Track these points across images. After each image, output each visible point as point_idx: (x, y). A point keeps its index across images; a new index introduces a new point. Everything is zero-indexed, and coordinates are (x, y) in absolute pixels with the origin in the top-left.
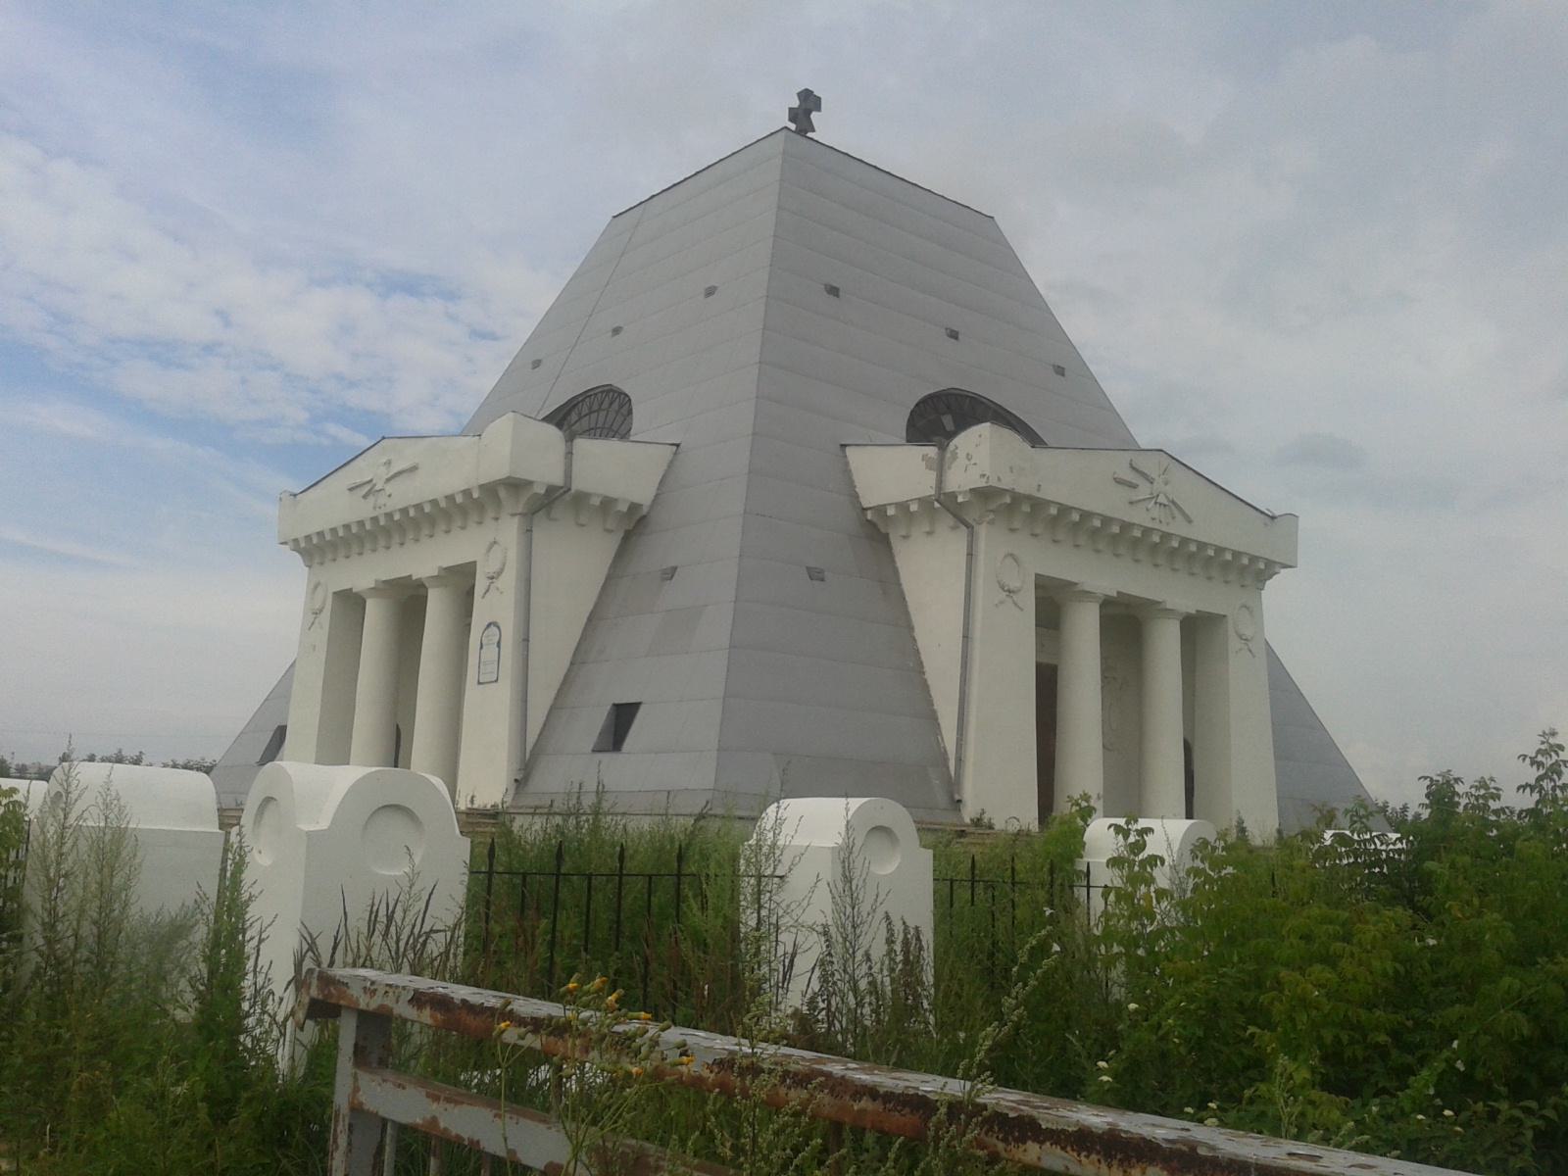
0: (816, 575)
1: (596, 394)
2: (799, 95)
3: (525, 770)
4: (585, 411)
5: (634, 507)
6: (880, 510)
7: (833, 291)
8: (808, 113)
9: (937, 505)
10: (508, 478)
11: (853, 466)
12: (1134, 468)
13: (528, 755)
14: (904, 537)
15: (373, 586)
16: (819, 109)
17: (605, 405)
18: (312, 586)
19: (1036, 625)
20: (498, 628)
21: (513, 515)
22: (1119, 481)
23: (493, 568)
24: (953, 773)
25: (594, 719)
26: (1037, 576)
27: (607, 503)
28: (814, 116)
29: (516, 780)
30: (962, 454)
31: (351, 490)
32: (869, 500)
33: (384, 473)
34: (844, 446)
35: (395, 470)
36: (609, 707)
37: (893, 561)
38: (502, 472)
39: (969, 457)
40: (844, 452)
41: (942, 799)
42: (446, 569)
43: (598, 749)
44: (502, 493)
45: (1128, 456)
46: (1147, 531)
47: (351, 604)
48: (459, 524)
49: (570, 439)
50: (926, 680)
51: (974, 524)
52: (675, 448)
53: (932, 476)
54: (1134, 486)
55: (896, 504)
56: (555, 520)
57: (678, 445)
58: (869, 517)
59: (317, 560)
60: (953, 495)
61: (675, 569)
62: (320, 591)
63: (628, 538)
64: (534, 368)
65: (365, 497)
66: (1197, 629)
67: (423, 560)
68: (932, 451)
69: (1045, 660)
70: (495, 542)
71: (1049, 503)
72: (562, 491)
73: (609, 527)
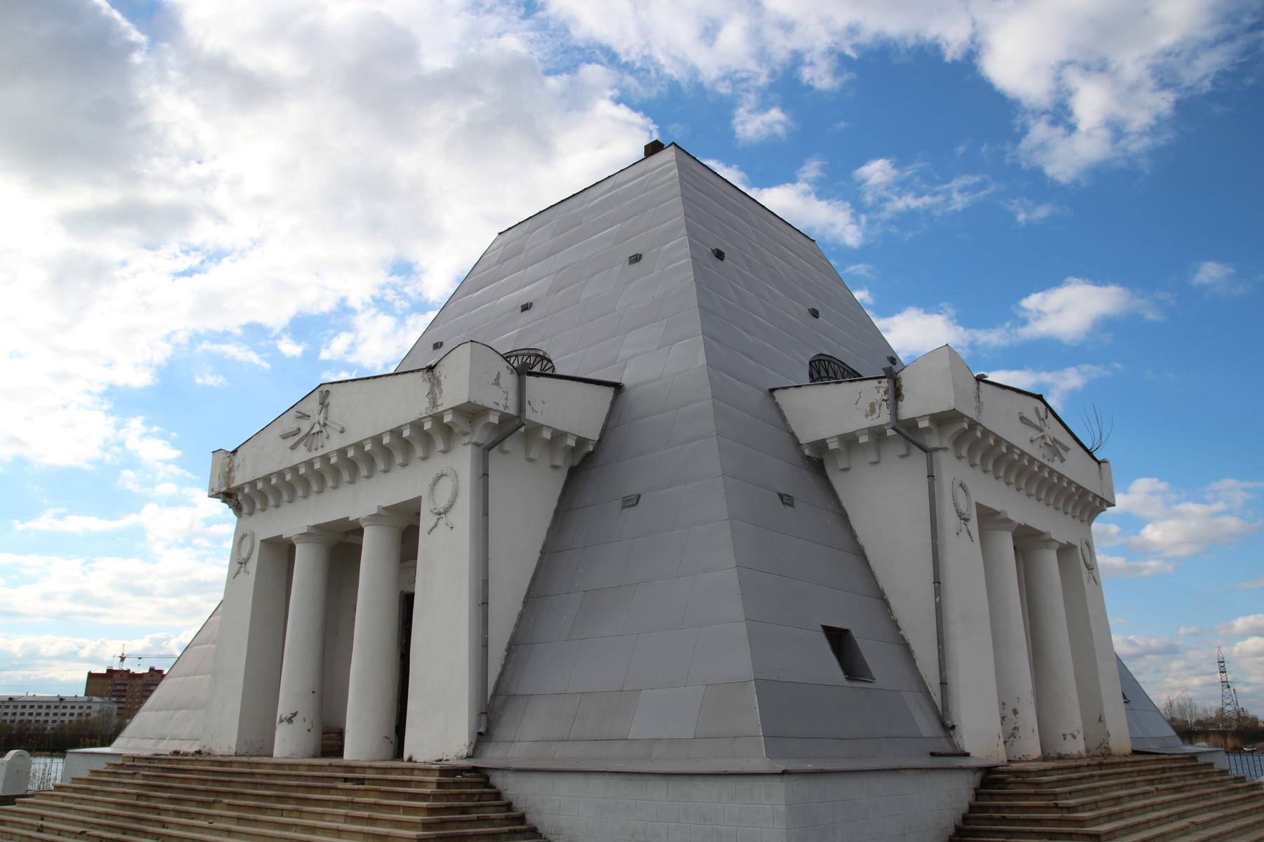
0: (786, 500)
5: (581, 442)
6: (821, 445)
14: (845, 470)
15: (305, 531)
18: (238, 539)
23: (442, 503)
24: (941, 713)
27: (558, 435)
32: (807, 435)
40: (774, 398)
42: (384, 508)
47: (282, 551)
52: (609, 392)
61: (639, 496)
62: (247, 541)
63: (573, 473)
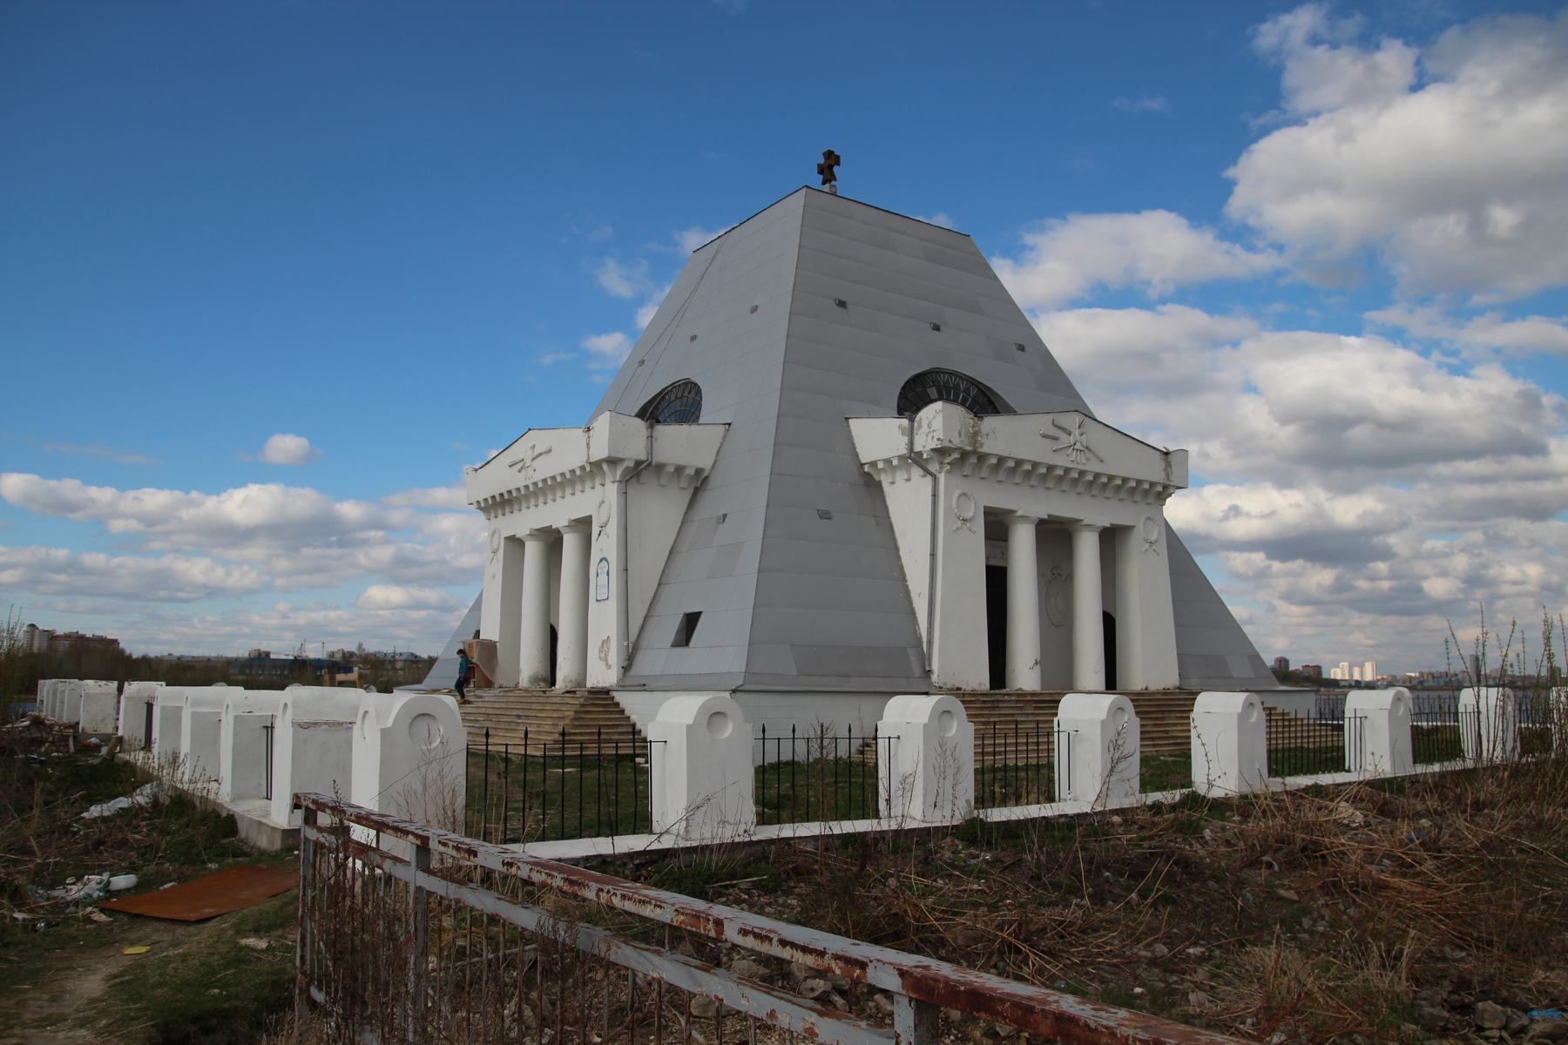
1: (679, 385)
2: (824, 154)
3: (629, 660)
4: (673, 398)
5: (699, 471)
6: (874, 464)
7: (842, 304)
8: (831, 167)
9: (910, 461)
10: (609, 457)
11: (854, 433)
12: (1056, 426)
13: (630, 650)
16: (838, 164)
17: (686, 394)
19: (987, 538)
20: (607, 561)
21: (613, 482)
22: (1045, 436)
23: (604, 519)
25: (673, 624)
26: (985, 507)
27: (679, 470)
28: (836, 169)
29: (623, 667)
30: (925, 423)
31: (510, 466)
33: (530, 455)
34: (847, 419)
35: (537, 451)
36: (682, 616)
37: (884, 501)
38: (604, 454)
39: (929, 426)
40: (848, 423)
41: (917, 672)
43: (676, 644)
44: (605, 466)
45: (1050, 417)
46: (1067, 470)
48: (580, 488)
49: (651, 427)
50: (907, 586)
51: (935, 473)
52: (727, 426)
53: (906, 439)
54: (1056, 439)
55: (884, 460)
56: (643, 484)
57: (729, 424)
58: (866, 470)
59: (493, 515)
60: (920, 454)
64: (752, 313)
65: (519, 471)
66: (1111, 538)
67: (558, 513)
68: (905, 422)
69: (994, 563)
70: (603, 502)
71: (988, 455)
72: (645, 464)
73: (682, 485)
